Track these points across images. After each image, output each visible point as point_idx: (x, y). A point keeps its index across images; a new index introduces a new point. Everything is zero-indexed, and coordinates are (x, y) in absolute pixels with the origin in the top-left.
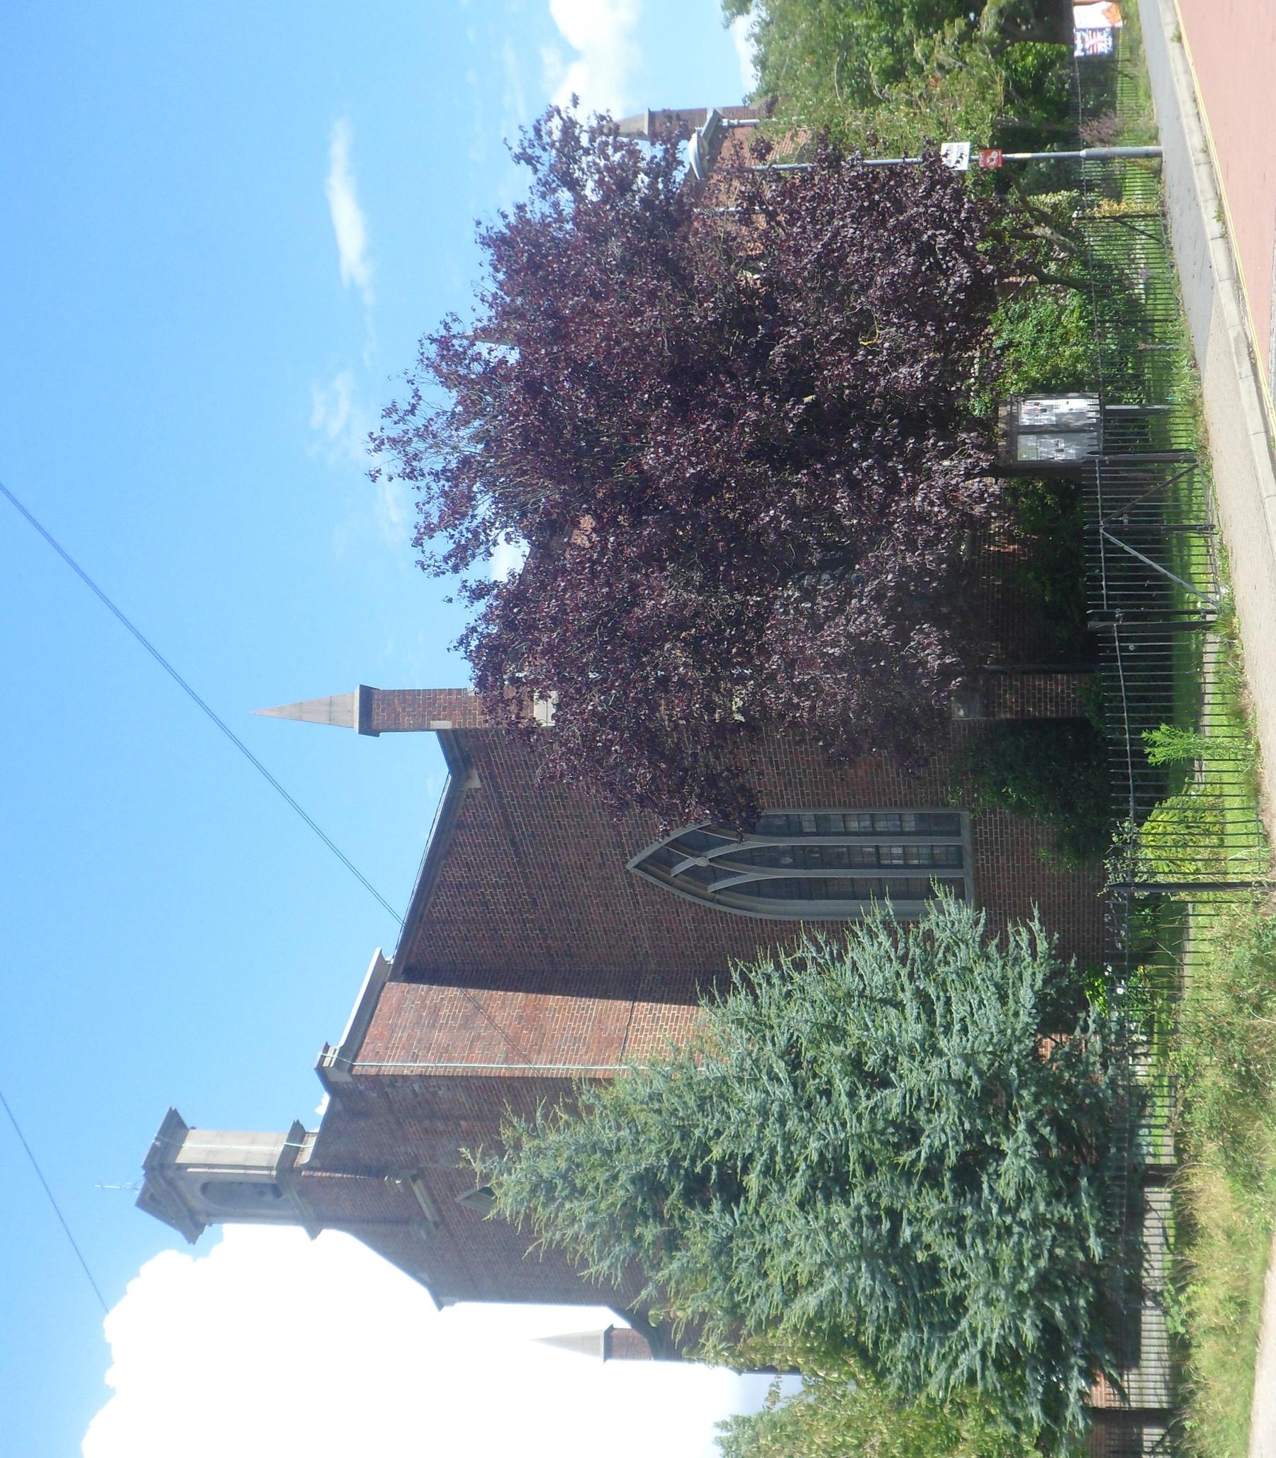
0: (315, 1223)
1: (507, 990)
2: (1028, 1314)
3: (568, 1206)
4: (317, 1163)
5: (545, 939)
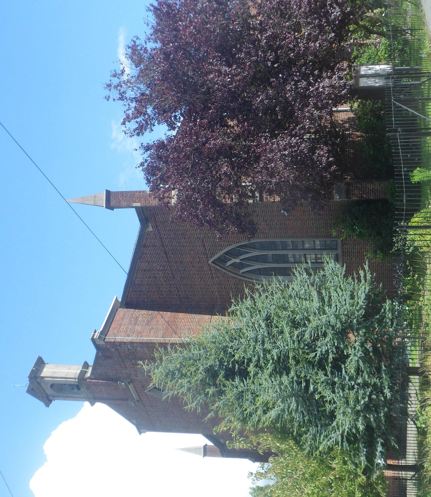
1: (164, 311)
2: (360, 419)
3: (180, 381)
4: (93, 377)
5: (178, 292)
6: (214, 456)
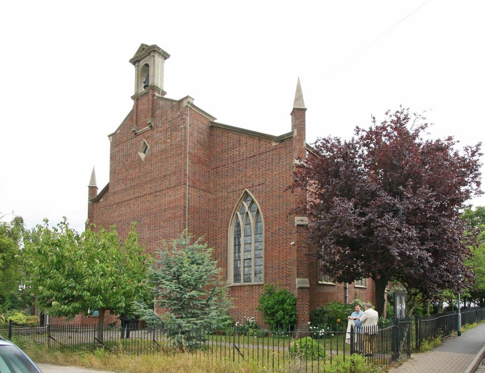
0: (136, 98)
5: (222, 166)
6: (89, 194)
